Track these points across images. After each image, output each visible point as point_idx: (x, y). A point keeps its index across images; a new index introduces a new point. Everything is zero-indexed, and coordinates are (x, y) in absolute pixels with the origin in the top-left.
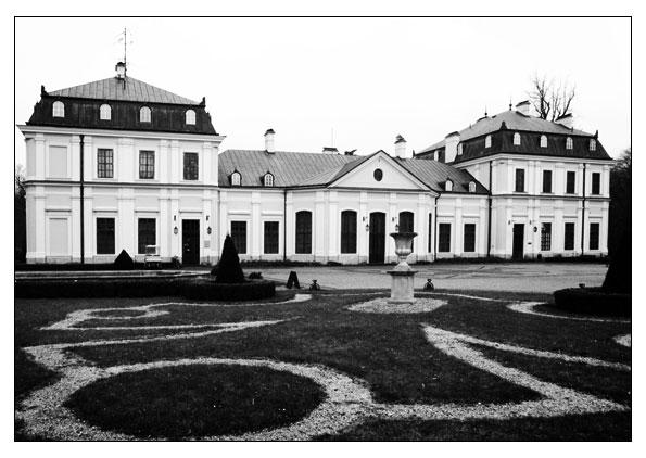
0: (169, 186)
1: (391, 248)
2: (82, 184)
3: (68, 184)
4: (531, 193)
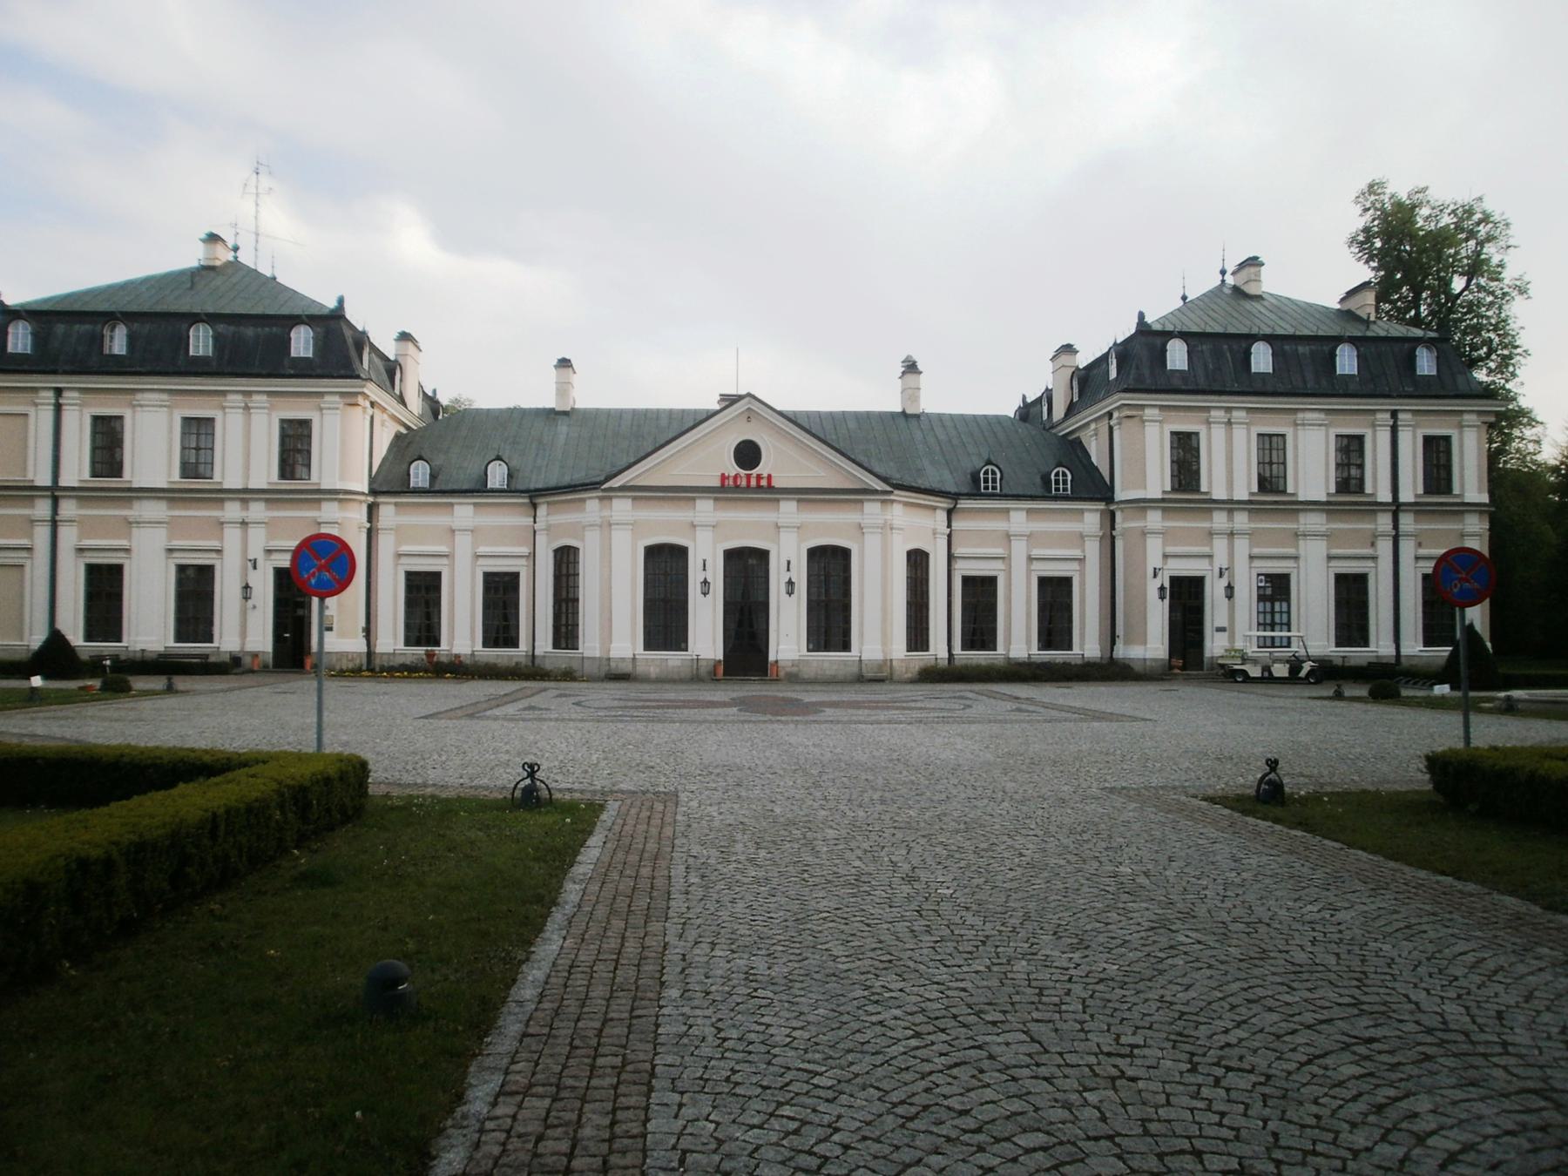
0: (245, 495)
2: (1396, 508)
3: (24, 492)
4: (1219, 493)
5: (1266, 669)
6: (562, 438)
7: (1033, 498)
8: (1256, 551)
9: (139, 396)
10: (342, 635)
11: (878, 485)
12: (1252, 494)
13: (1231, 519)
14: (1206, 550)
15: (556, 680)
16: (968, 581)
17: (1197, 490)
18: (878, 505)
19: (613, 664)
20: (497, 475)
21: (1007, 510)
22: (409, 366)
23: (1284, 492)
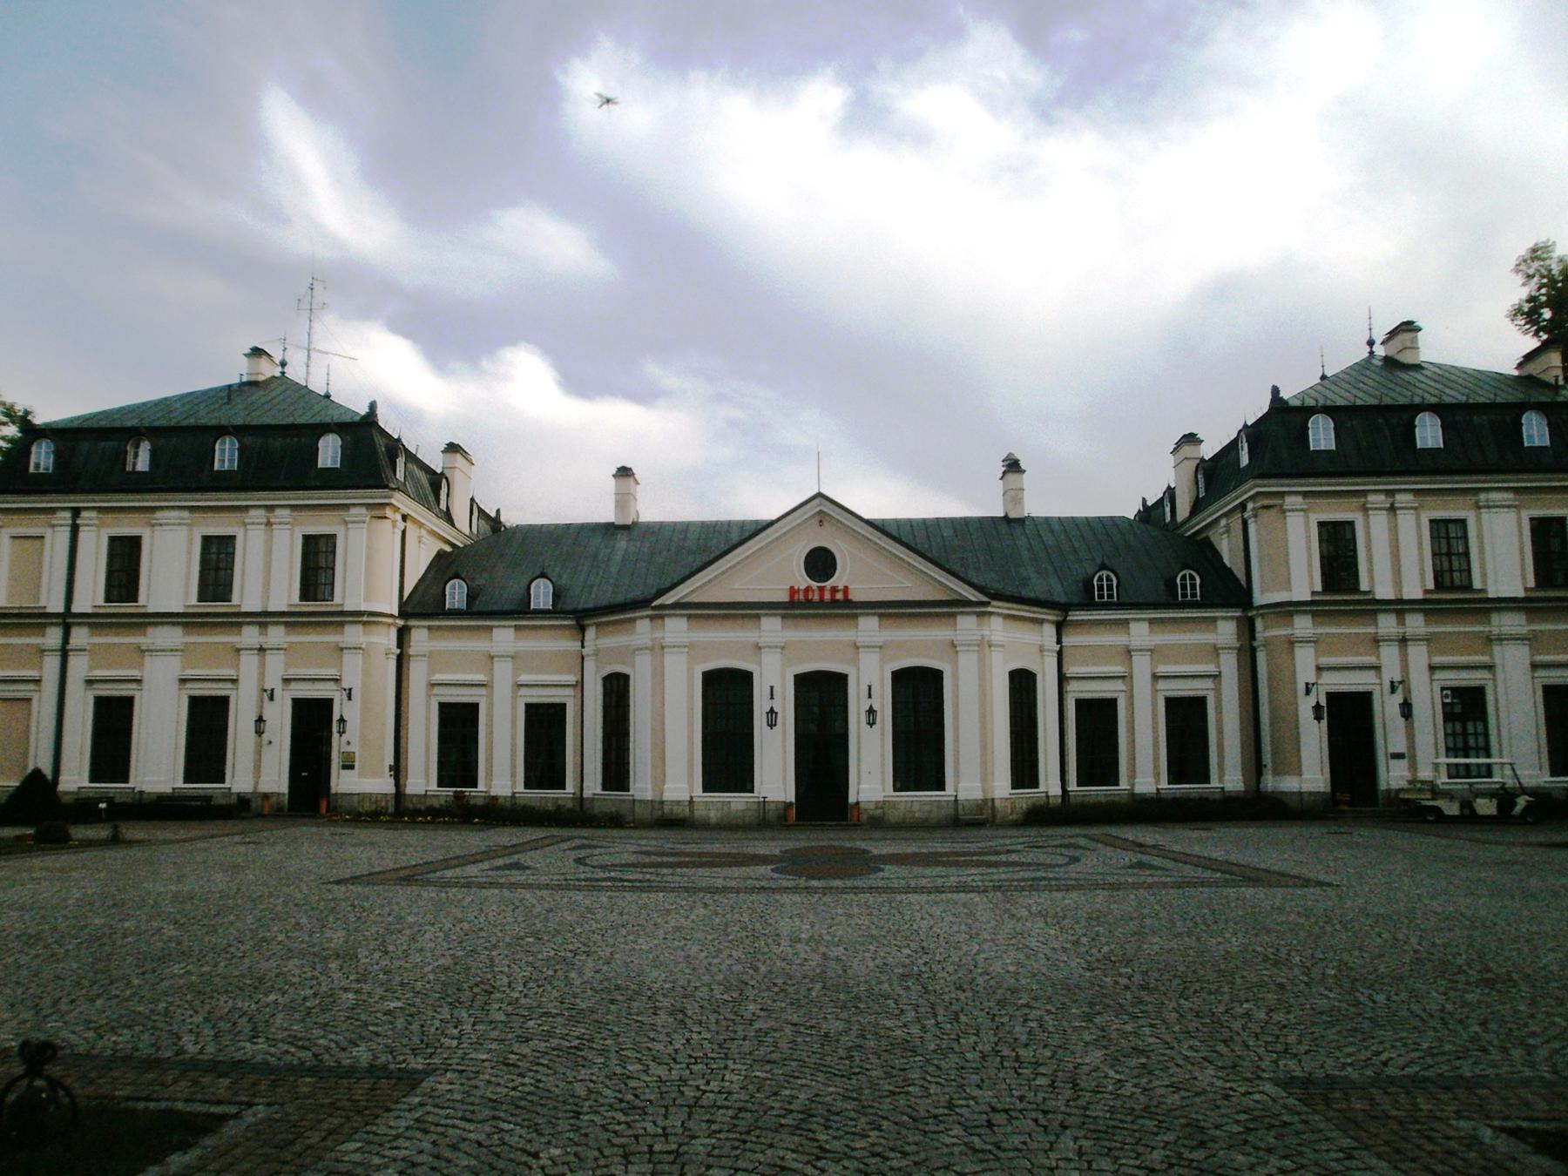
0: (263, 619)
1: (870, 774)
3: (32, 620)
4: (1384, 592)
5: (1466, 805)
6: (618, 557)
7: (1156, 606)
8: (1437, 660)
9: (159, 514)
10: (363, 775)
12: (1427, 591)
13: (1401, 622)
15: (599, 826)
16: (1081, 704)
17: (1355, 589)
18: (974, 618)
19: (666, 808)
20: (542, 593)
21: (1127, 621)
22: (457, 479)
23: (1468, 587)
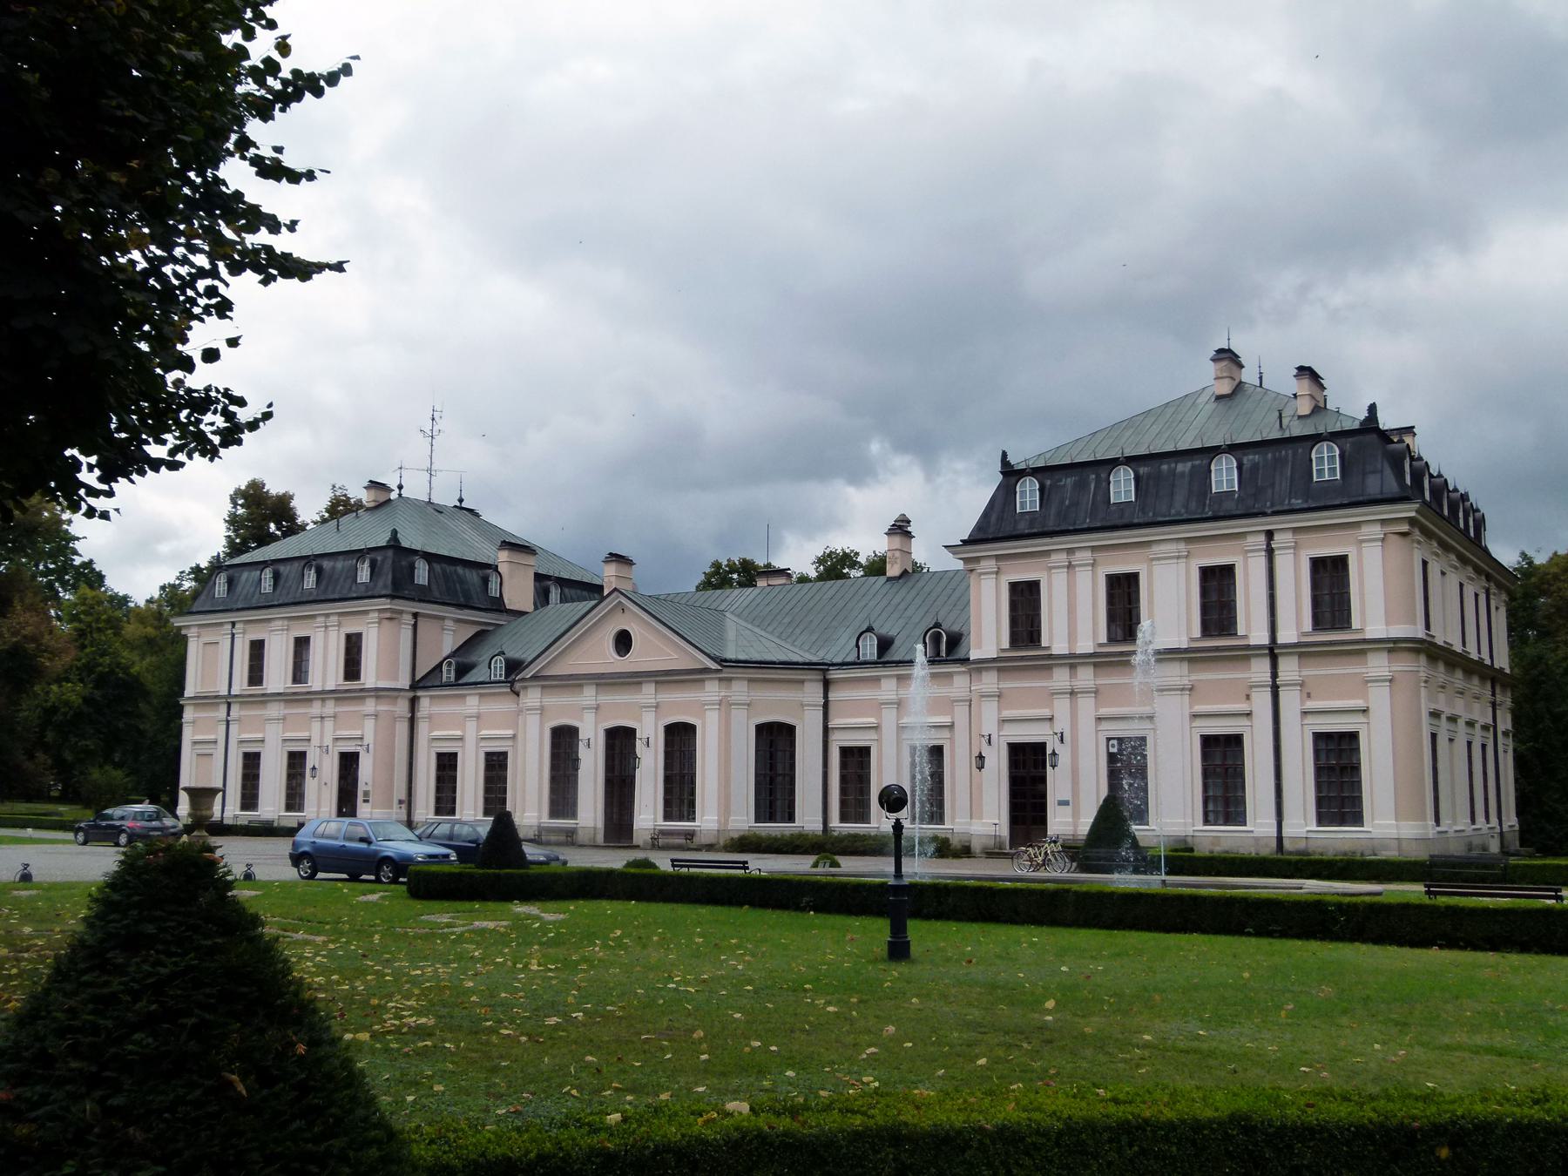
0: (1073, 661)
2: (1273, 652)
11: (714, 666)
14: (1046, 712)
16: (846, 752)
